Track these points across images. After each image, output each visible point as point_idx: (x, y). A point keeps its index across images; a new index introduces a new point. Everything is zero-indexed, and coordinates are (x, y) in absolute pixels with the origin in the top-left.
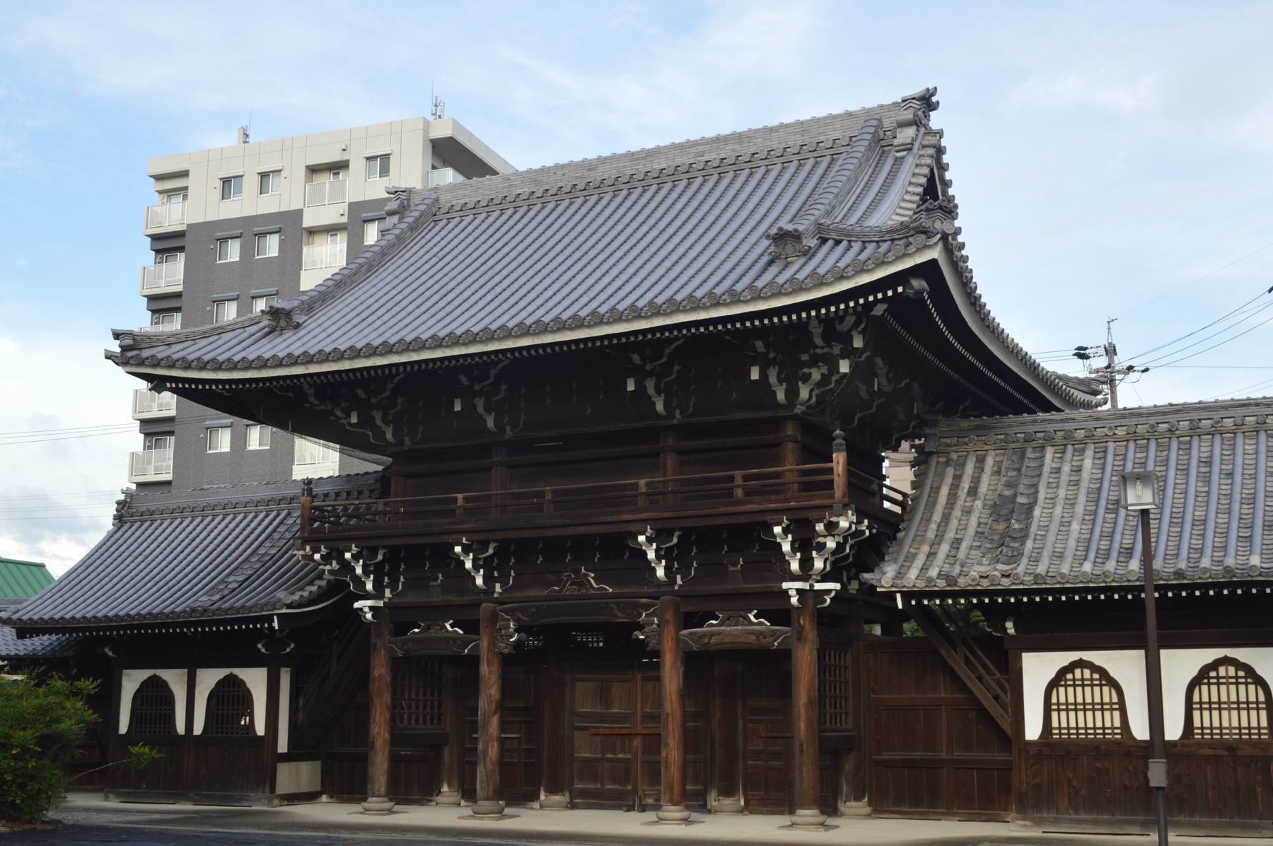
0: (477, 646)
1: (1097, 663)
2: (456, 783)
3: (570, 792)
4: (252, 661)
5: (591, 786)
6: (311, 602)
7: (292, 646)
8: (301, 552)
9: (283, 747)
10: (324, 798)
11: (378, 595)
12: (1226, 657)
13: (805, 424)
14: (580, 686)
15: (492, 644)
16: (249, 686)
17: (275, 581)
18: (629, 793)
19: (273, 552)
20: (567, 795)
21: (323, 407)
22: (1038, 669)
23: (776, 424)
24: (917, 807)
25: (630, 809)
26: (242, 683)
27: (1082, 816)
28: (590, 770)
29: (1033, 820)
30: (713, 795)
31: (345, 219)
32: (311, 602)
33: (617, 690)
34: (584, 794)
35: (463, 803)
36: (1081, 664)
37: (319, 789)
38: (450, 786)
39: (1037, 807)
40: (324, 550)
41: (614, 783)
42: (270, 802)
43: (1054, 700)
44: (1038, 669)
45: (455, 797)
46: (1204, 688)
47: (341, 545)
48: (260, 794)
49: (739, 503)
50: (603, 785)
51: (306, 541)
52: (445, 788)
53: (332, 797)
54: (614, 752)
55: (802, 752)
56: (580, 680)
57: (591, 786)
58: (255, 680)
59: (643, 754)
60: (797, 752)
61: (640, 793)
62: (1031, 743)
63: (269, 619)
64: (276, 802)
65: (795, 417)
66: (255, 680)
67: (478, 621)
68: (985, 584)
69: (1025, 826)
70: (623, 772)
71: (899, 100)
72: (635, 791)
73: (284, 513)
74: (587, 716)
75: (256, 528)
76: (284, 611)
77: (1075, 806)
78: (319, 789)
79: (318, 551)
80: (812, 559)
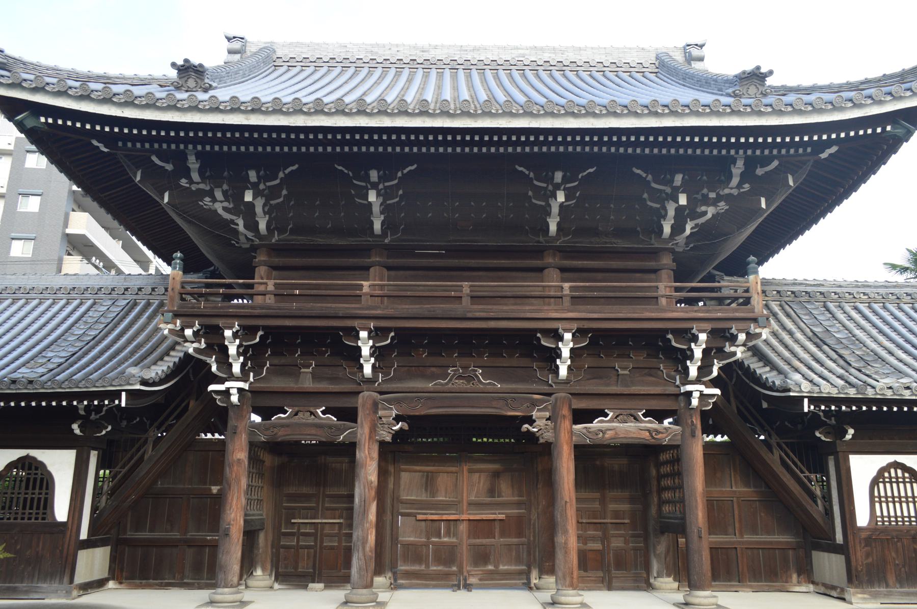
0: (355, 433)
1: (908, 465)
2: (269, 566)
3: (394, 574)
4: (58, 440)
5: (416, 568)
6: (161, 382)
7: (109, 428)
8: (170, 326)
9: (84, 535)
10: (111, 584)
11: (244, 377)
12: (896, 462)
13: (677, 258)
14: (405, 477)
15: (373, 429)
16: (50, 468)
17: (111, 358)
18: (453, 574)
19: (93, 333)
20: (389, 575)
21: (202, 186)
22: (863, 468)
23: (654, 253)
24: (729, 581)
25: (457, 587)
26: (41, 466)
27: (906, 590)
28: (414, 553)
29: (870, 594)
30: (534, 574)
31: (11, 147)
32: (161, 382)
33: (444, 480)
34: (408, 575)
35: (276, 586)
36: (897, 465)
37: (106, 575)
38: (264, 569)
39: (871, 583)
40: (197, 327)
41: (439, 565)
42: (68, 594)
43: (876, 494)
44: (863, 468)
45: (269, 581)
46: (881, 485)
47: (221, 322)
48: (55, 585)
49: (665, 311)
50: (427, 566)
51: (177, 315)
52: (259, 572)
53: (121, 583)
54: (439, 536)
55: (700, 537)
56: (405, 471)
57: (416, 568)
58: (60, 464)
59: (469, 537)
60: (696, 538)
61: (465, 574)
62: (861, 529)
63: (117, 394)
64: (75, 593)
65: (672, 251)
66: (60, 464)
67: (356, 408)
68: (889, 394)
69: (864, 598)
70: (447, 556)
71: (649, 59)
72: (461, 571)
73: (89, 303)
74: (412, 503)
75: (57, 313)
76: (138, 387)
77: (901, 582)
78: (106, 575)
79: (191, 327)
80: (687, 368)
